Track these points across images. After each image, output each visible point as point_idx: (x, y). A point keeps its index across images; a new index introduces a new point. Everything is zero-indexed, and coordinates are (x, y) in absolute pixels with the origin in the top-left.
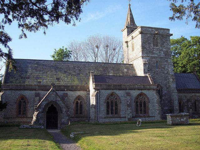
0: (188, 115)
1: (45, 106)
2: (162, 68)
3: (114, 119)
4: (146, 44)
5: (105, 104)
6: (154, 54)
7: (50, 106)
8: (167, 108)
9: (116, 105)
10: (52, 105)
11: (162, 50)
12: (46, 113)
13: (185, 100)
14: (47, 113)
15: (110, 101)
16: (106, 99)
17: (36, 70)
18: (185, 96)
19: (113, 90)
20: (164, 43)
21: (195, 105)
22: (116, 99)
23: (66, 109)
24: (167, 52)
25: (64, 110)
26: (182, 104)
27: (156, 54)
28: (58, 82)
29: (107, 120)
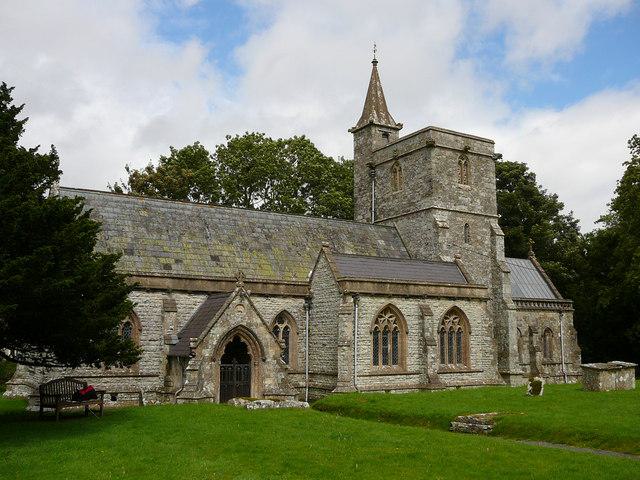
0: (632, 367)
1: (219, 342)
5: (371, 338)
6: (459, 202)
10: (237, 339)
14: (224, 360)
17: (147, 227)
18: (525, 318)
28: (218, 269)
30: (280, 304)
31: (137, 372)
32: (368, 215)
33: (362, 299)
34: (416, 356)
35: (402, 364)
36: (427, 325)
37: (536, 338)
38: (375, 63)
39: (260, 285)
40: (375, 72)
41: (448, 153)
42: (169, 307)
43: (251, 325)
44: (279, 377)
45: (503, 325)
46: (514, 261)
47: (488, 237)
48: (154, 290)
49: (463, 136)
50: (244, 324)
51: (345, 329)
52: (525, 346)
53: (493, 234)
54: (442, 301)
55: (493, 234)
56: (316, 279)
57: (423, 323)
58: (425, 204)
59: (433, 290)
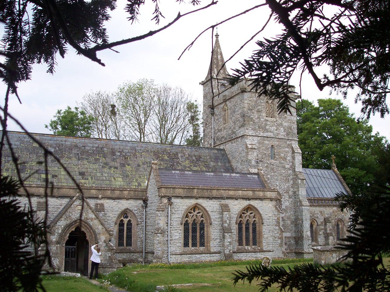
1: (63, 231)
2: (281, 158)
3: (198, 256)
4: (253, 113)
5: (182, 228)
6: (267, 131)
7: (74, 229)
8: (288, 234)
9: (202, 229)
10: (78, 229)
11: (281, 125)
12: (64, 245)
13: (321, 220)
14: (68, 243)
15: (244, 221)
16: (183, 217)
18: (321, 212)
21: (338, 228)
22: (202, 217)
24: (290, 128)
26: (314, 227)
27: (271, 132)
29: (185, 259)
30: (124, 204)
32: (210, 142)
34: (218, 240)
36: (225, 219)
37: (329, 226)
39: (109, 192)
42: (225, 208)
43: (87, 219)
44: (108, 255)
45: (299, 217)
46: (311, 171)
47: (290, 154)
52: (321, 233)
53: (293, 152)
54: (239, 201)
55: (293, 152)
56: (149, 187)
57: (222, 217)
58: (241, 132)
59: (231, 193)
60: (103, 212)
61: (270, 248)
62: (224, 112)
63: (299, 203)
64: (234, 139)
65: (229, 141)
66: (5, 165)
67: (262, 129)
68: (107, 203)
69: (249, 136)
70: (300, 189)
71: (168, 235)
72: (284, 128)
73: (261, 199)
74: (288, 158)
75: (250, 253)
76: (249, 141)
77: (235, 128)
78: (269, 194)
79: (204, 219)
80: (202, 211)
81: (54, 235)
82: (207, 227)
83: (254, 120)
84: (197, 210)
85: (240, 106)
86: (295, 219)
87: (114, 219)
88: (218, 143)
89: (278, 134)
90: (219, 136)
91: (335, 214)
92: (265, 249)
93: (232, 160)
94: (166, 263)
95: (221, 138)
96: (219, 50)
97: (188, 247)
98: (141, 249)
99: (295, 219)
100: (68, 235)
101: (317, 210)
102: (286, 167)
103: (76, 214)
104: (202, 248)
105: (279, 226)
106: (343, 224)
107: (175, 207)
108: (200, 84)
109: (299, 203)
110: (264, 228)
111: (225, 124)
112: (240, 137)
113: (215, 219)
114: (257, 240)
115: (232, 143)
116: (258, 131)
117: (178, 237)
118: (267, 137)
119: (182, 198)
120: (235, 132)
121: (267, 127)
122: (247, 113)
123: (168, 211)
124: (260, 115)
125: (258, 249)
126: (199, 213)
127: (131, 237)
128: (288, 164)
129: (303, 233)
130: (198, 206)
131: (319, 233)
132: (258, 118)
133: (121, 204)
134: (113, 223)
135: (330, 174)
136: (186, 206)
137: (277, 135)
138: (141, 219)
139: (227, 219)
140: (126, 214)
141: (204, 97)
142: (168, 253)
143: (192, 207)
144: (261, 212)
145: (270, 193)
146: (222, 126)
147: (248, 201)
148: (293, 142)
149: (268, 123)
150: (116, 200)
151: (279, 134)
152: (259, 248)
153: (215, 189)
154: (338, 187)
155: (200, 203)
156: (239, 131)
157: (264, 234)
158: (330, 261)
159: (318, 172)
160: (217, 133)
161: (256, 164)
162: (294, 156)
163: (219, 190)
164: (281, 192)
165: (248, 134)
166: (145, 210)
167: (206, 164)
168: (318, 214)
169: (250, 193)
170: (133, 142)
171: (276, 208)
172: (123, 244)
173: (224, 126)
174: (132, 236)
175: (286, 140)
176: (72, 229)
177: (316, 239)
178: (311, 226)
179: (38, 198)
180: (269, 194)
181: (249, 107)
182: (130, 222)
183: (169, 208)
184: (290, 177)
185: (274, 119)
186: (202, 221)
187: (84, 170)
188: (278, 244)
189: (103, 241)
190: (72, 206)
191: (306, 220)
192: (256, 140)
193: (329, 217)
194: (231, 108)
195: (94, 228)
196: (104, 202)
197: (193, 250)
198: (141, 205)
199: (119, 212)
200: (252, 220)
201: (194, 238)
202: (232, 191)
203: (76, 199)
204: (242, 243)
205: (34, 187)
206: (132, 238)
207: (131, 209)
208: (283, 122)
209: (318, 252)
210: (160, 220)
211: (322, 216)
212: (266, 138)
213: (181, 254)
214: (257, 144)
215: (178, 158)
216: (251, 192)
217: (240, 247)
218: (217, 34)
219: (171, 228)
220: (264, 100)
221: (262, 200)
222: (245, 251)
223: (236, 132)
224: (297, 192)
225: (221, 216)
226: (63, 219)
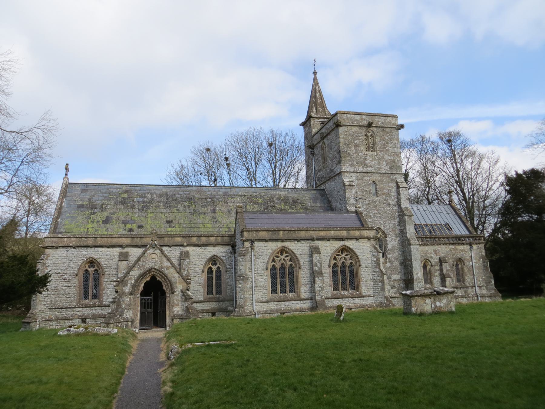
1: (136, 281)
2: (385, 194)
3: (287, 303)
4: (350, 148)
5: (205, 275)
7: (148, 279)
9: (292, 274)
10: (153, 278)
11: (383, 158)
12: (139, 295)
13: (435, 260)
14: (143, 294)
18: (435, 251)
19: (282, 241)
20: (387, 143)
22: (290, 260)
23: (183, 286)
25: (179, 287)
26: (428, 268)
27: (371, 167)
30: (212, 251)
31: (102, 303)
33: (256, 244)
35: (297, 293)
38: (315, 73)
40: (316, 82)
41: (355, 129)
42: (314, 250)
43: (162, 267)
45: (408, 258)
48: (113, 246)
49: (368, 115)
50: (157, 267)
51: (242, 267)
54: (331, 242)
57: (312, 260)
60: (188, 260)
61: (371, 292)
62: (323, 151)
63: (407, 242)
64: (332, 178)
65: (328, 180)
66: (91, 217)
67: (360, 165)
68: (193, 251)
69: (346, 173)
70: (407, 226)
71: (252, 281)
72: (386, 162)
73: (357, 239)
74: (393, 194)
75: (347, 299)
76: (347, 177)
77: (332, 166)
78: (366, 233)
79: (293, 263)
80: (290, 255)
81: (127, 285)
82: (296, 271)
83: (352, 155)
84: (285, 253)
85: (336, 142)
86: (403, 260)
87: (202, 267)
88: (319, 183)
89: (380, 168)
90: (319, 176)
91: (453, 253)
92: (364, 294)
93: (331, 200)
94: (250, 312)
95: (322, 178)
96: (317, 88)
97: (277, 293)
98: (231, 297)
99: (403, 260)
100: (143, 285)
101: (430, 249)
102: (391, 204)
103: (149, 263)
104: (291, 295)
105: (379, 268)
106: (463, 263)
107: (259, 251)
108: (300, 125)
109: (407, 242)
110: (362, 271)
111: (324, 163)
112: (337, 175)
113: (305, 263)
114: (355, 284)
115: (331, 182)
116: (357, 167)
117: (263, 283)
118: (367, 173)
119: (266, 241)
120: (333, 170)
121: (367, 162)
122: (343, 149)
123: (252, 256)
124: (358, 150)
125: (356, 294)
126: (347, 255)
127: (221, 284)
128: (393, 201)
129: (413, 274)
130: (285, 249)
131: (434, 274)
132: (356, 153)
133: (208, 251)
134: (199, 271)
135: (447, 209)
136: (272, 250)
137: (379, 170)
138: (230, 265)
139: (317, 262)
140: (215, 261)
141: (305, 138)
142: (253, 300)
143: (279, 250)
144: (358, 253)
145: (367, 231)
146: (321, 166)
147: (342, 242)
148: (397, 176)
149: (368, 157)
150: (202, 247)
151: (381, 168)
152: (358, 293)
153: (303, 231)
154: (456, 223)
155: (287, 246)
156: (337, 168)
157: (363, 277)
158: (422, 308)
159: (432, 208)
160: (318, 173)
161: (354, 202)
162: (399, 191)
163: (308, 231)
164: (386, 231)
165: (345, 171)
166: (234, 256)
167: (303, 206)
168: (432, 253)
169: (344, 233)
170: (226, 188)
171: (375, 248)
172: (213, 292)
173: (324, 165)
174: (222, 284)
175: (389, 175)
176: (147, 278)
177: (431, 281)
178: (425, 267)
179: (120, 248)
180: (366, 233)
181: (345, 142)
182: (274, 267)
183: (253, 253)
184: (396, 214)
185: (375, 153)
186: (291, 265)
187: (171, 219)
188: (379, 288)
189: (180, 290)
190: (146, 255)
191: (416, 260)
192: (354, 177)
193: (447, 257)
194: (328, 145)
195: (170, 276)
196: (190, 249)
197: (282, 297)
198: (229, 251)
199: (206, 259)
200: (348, 263)
201: (283, 284)
202: (323, 232)
203: (150, 247)
204: (338, 287)
205: (116, 237)
206: (222, 286)
207: (219, 255)
208: (385, 155)
209: (407, 297)
210: (242, 265)
211: (437, 255)
212: (366, 174)
213: (267, 302)
214: (356, 181)
215: (274, 201)
216: (345, 232)
217: (335, 292)
218: (315, 71)
219: (256, 274)
220: (362, 133)
221: (359, 240)
222: (341, 296)
223: (334, 170)
224: (404, 230)
225: (311, 259)
226: (136, 269)
